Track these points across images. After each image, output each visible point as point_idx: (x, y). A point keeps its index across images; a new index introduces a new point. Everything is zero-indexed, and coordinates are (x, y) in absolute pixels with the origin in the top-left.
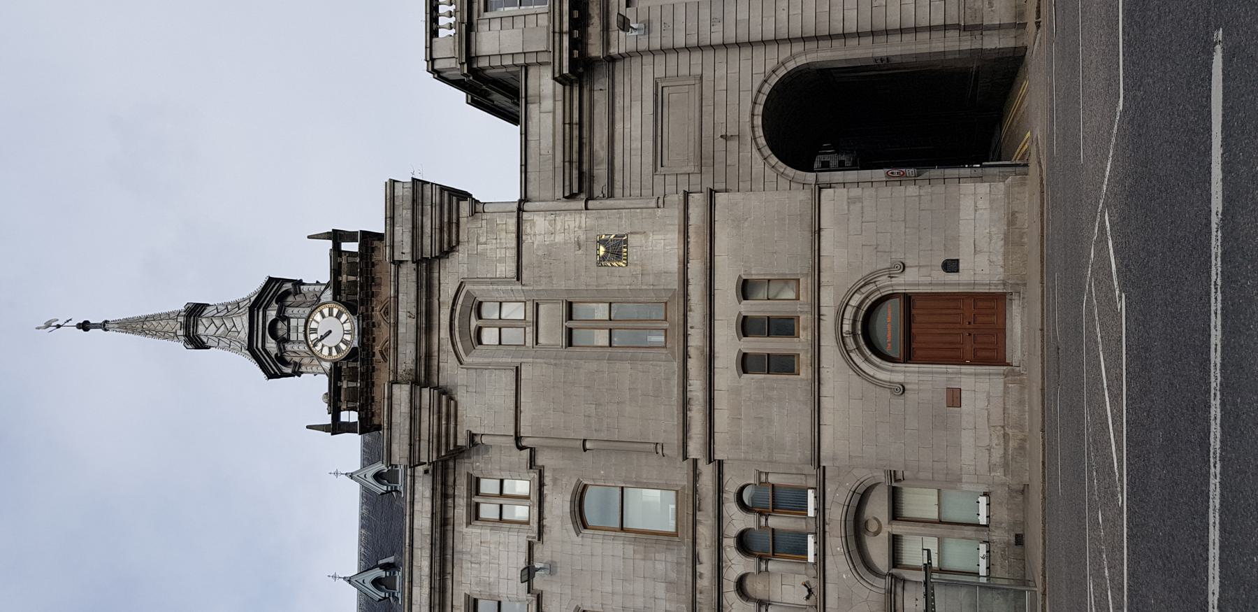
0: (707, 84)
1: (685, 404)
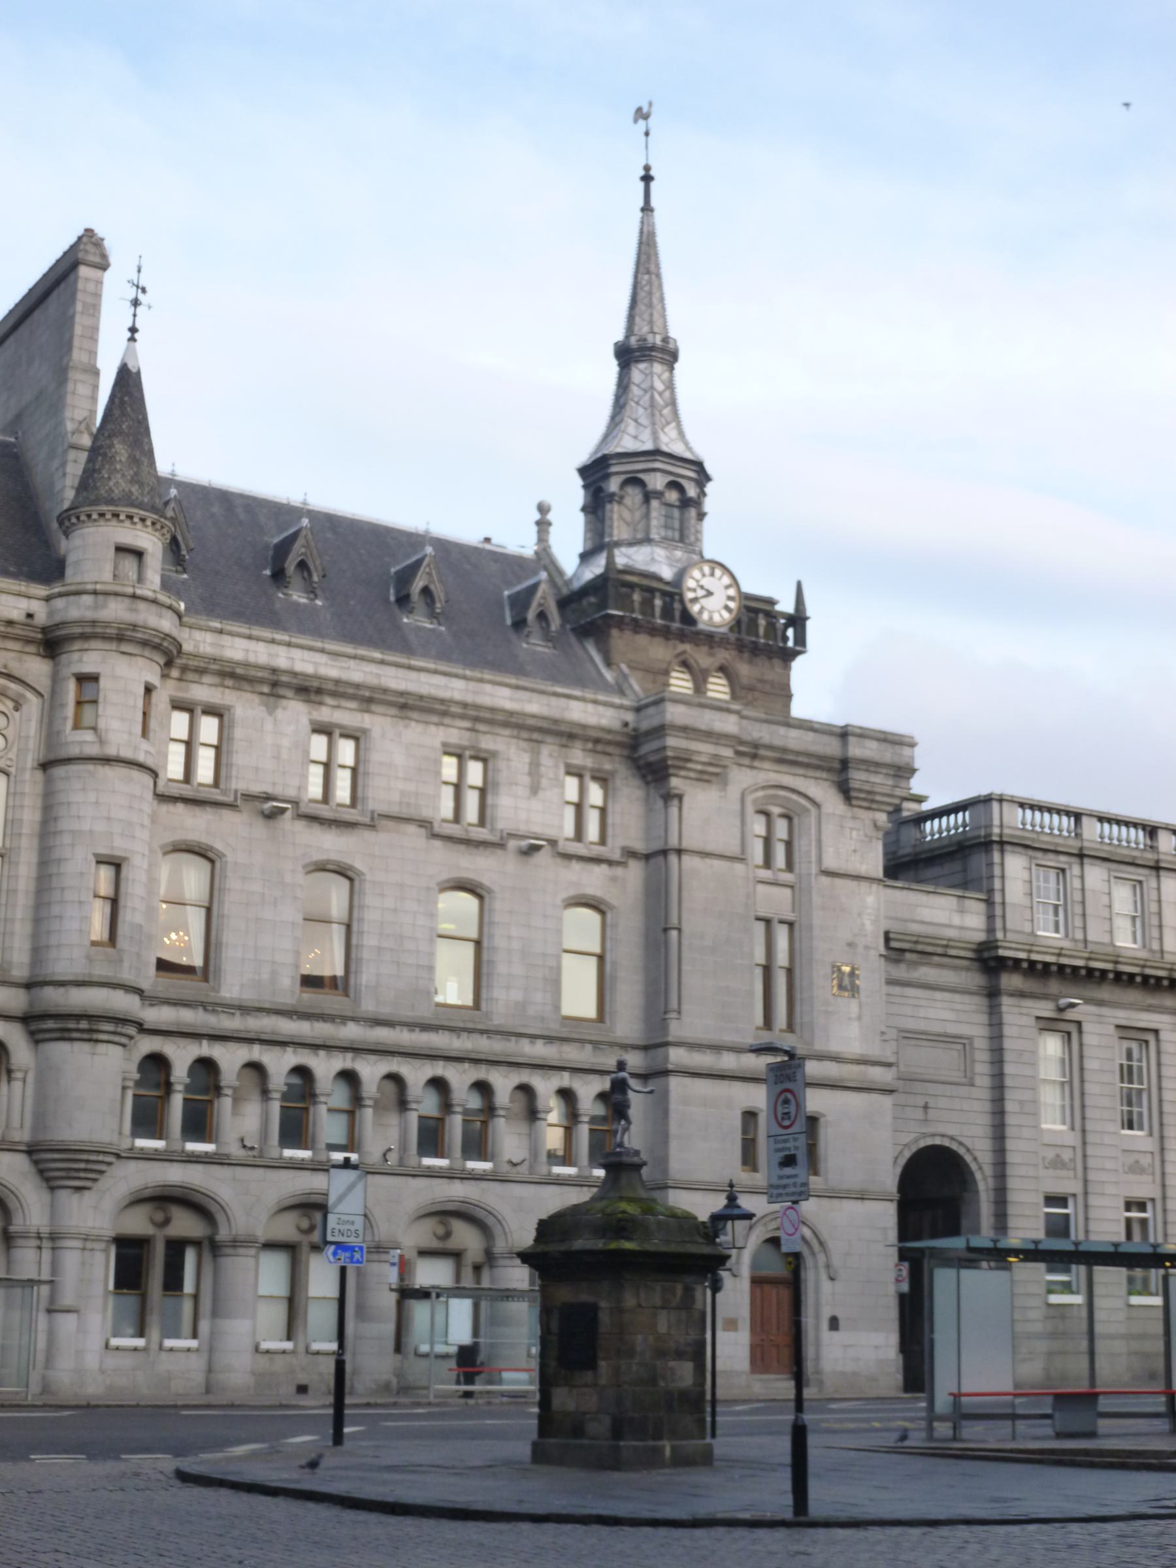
0: (964, 1091)
1: (717, 1048)
